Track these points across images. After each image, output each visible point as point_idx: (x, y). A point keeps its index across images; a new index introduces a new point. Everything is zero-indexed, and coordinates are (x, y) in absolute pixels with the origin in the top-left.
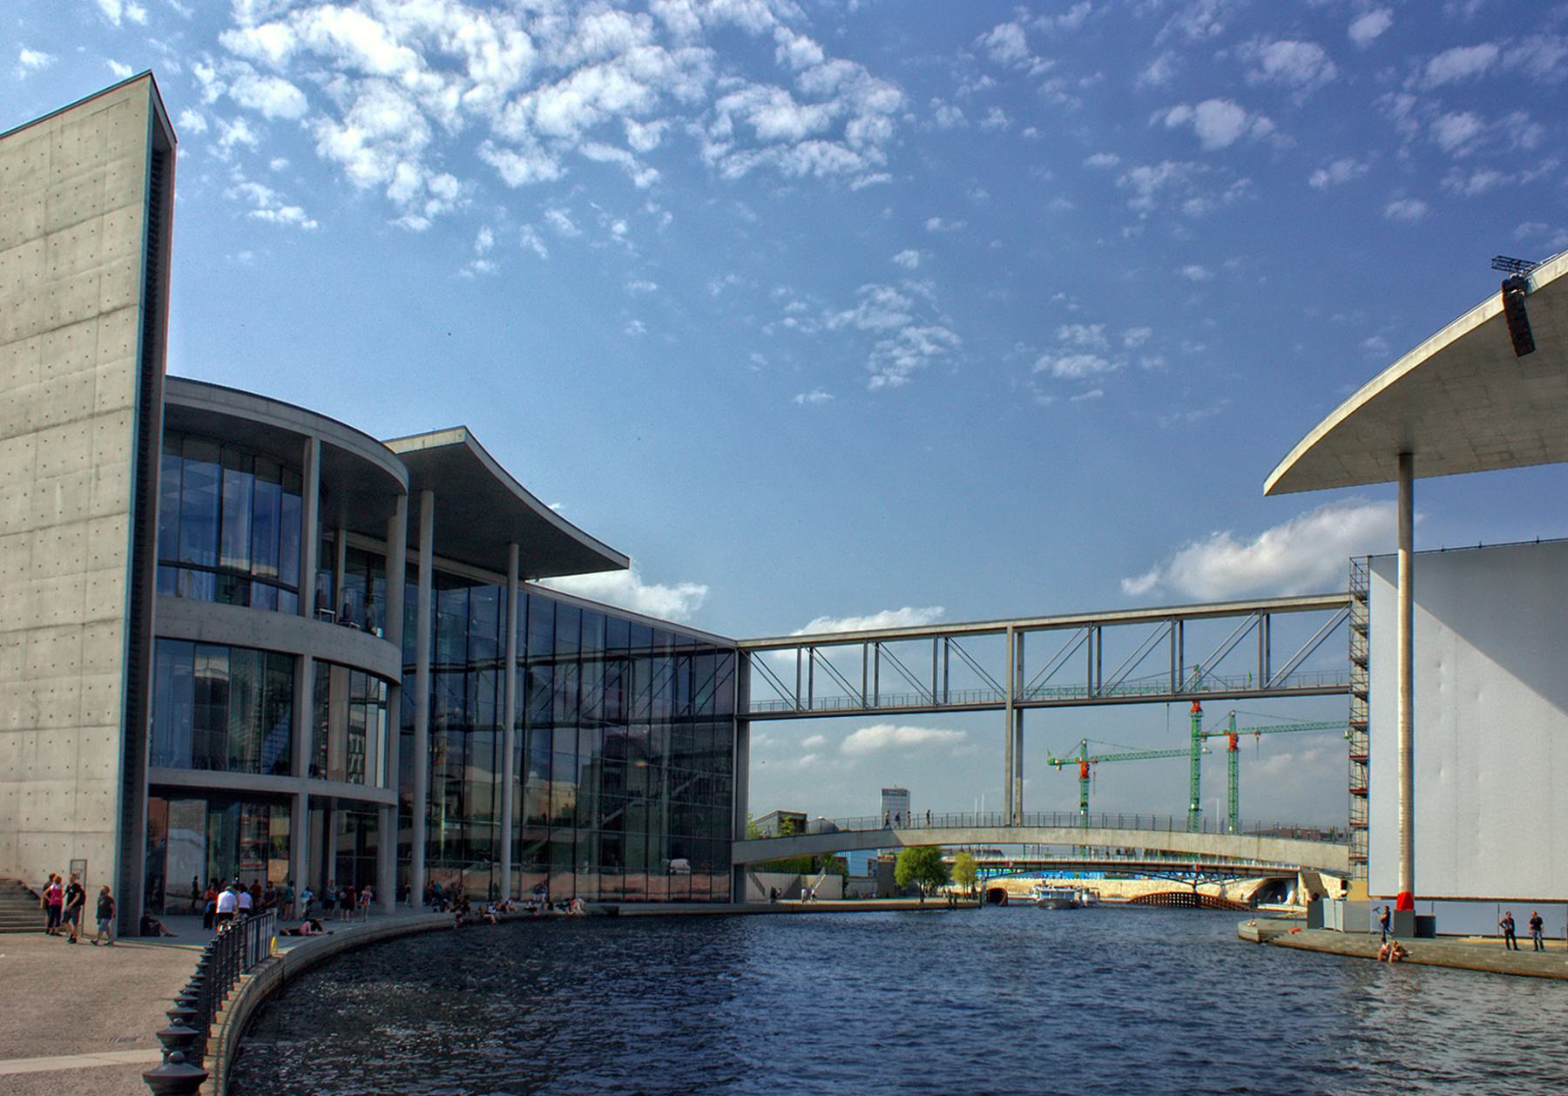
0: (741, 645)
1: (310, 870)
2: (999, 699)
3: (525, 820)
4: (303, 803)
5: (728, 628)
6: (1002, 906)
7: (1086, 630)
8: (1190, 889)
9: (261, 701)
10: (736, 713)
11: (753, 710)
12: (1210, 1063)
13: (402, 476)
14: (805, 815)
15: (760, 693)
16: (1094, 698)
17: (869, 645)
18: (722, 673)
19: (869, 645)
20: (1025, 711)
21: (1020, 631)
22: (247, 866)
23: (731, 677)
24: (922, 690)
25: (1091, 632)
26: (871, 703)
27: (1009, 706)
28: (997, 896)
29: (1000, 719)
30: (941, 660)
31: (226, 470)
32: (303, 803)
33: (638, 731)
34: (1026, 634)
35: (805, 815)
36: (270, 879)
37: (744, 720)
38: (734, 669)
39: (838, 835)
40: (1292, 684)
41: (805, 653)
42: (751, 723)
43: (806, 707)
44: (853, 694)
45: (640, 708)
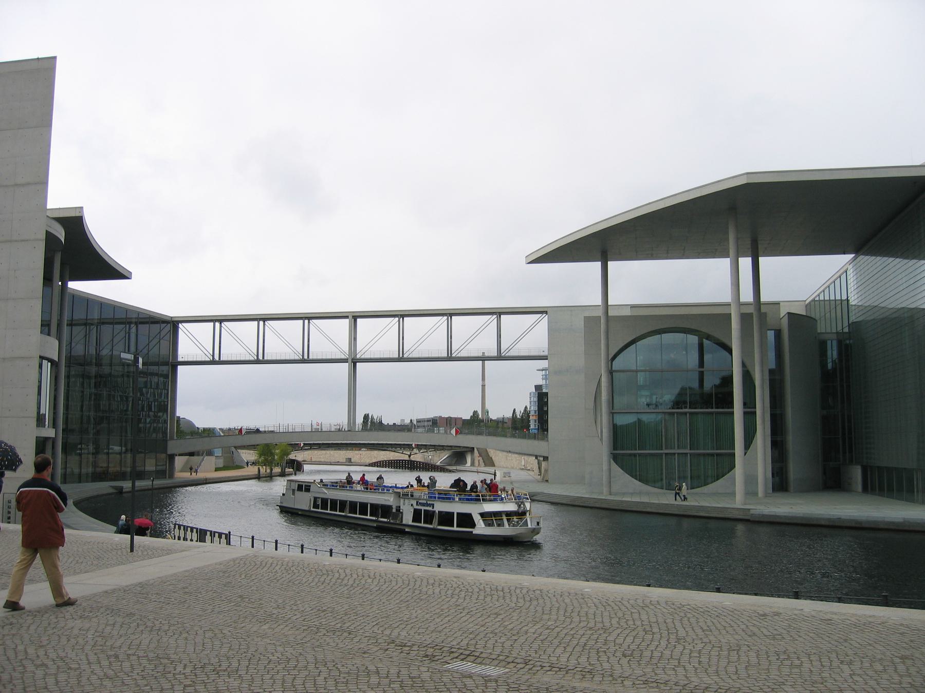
0: (174, 319)
1: (762, 352)
2: (343, 357)
3: (359, 420)
7: (397, 319)
8: (406, 458)
9: (399, 488)
11: (180, 359)
17: (260, 322)
18: (163, 334)
19: (260, 322)
23: (169, 334)
26: (217, 358)
27: (350, 361)
29: (345, 366)
31: (43, 360)
34: (358, 320)
36: (54, 429)
38: (170, 331)
39: (260, 435)
40: (512, 353)
41: (217, 324)
42: (179, 366)
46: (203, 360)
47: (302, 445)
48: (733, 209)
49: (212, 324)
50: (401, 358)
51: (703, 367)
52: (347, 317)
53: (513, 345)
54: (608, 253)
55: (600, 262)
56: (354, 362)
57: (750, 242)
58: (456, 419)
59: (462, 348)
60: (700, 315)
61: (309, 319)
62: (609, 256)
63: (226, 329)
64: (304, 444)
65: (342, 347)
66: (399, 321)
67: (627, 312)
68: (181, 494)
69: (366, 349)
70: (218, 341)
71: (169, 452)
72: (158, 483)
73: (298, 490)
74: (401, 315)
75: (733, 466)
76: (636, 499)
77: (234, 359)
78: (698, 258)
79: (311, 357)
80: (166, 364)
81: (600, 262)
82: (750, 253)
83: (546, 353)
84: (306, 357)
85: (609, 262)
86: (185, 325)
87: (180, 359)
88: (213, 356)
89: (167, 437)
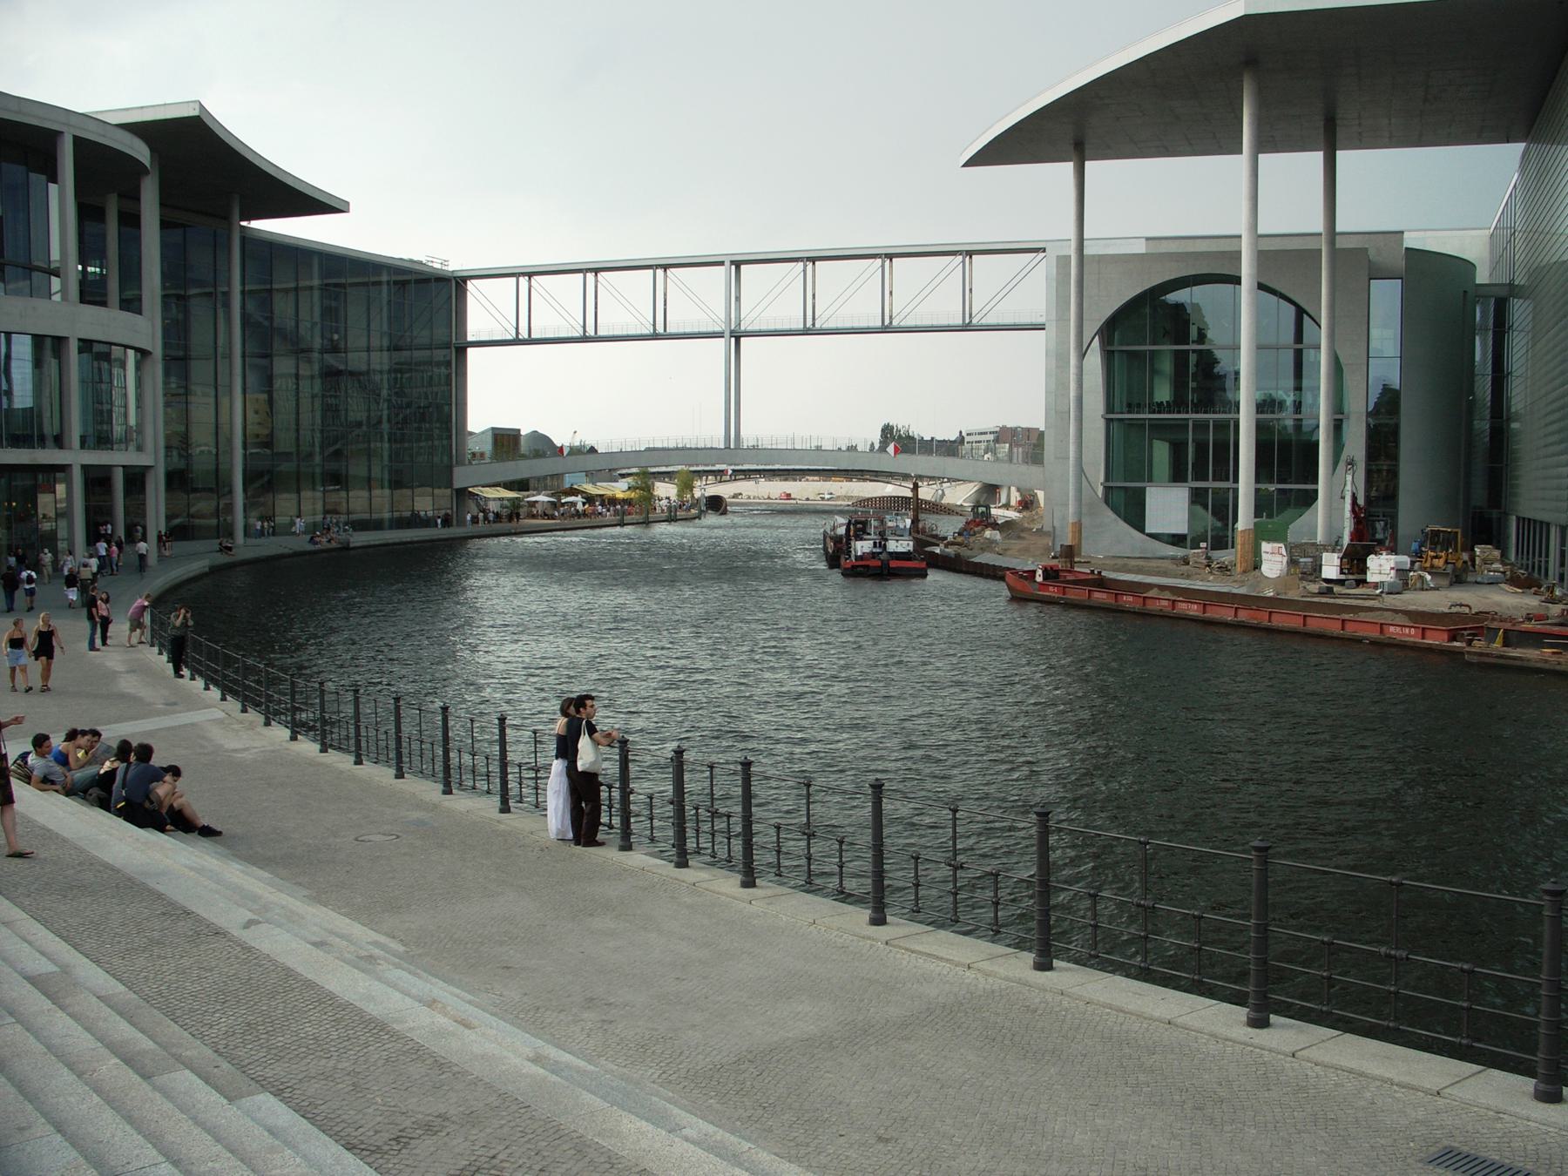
2: (717, 329)
4: (73, 346)
5: (454, 261)
6: (722, 514)
7: (879, 261)
10: (454, 341)
11: (470, 338)
12: (1294, 783)
13: (140, 151)
14: (519, 430)
15: (478, 323)
16: (809, 329)
20: (742, 339)
21: (738, 264)
22: (100, 369)
24: (714, 317)
25: (805, 266)
26: (590, 332)
27: (727, 334)
28: (716, 504)
30: (497, 315)
32: (73, 346)
33: (356, 361)
34: (742, 267)
35: (519, 430)
37: (461, 351)
43: (592, 334)
44: (572, 321)
45: (356, 339)
46: (570, 335)
47: (730, 472)
48: (1251, 62)
49: (514, 279)
50: (887, 327)
51: (1301, 343)
52: (721, 263)
53: (993, 303)
54: (1086, 146)
55: (1071, 164)
56: (737, 336)
57: (1322, 123)
58: (1029, 430)
59: (988, 308)
60: (1277, 252)
61: (666, 267)
62: (1087, 152)
63: (543, 292)
64: (734, 471)
65: (714, 315)
66: (963, 262)
67: (1140, 248)
68: (462, 556)
69: (907, 310)
70: (660, 302)
71: (457, 484)
72: (439, 532)
73: (1500, 508)
74: (967, 251)
75: (1316, 499)
76: (1076, 597)
77: (688, 330)
78: (1278, 151)
79: (818, 325)
80: (448, 346)
81: (1071, 164)
82: (1149, 251)
83: (1041, 320)
84: (809, 324)
85: (1338, 152)
86: (474, 281)
87: (470, 338)
88: (654, 325)
89: (451, 462)
